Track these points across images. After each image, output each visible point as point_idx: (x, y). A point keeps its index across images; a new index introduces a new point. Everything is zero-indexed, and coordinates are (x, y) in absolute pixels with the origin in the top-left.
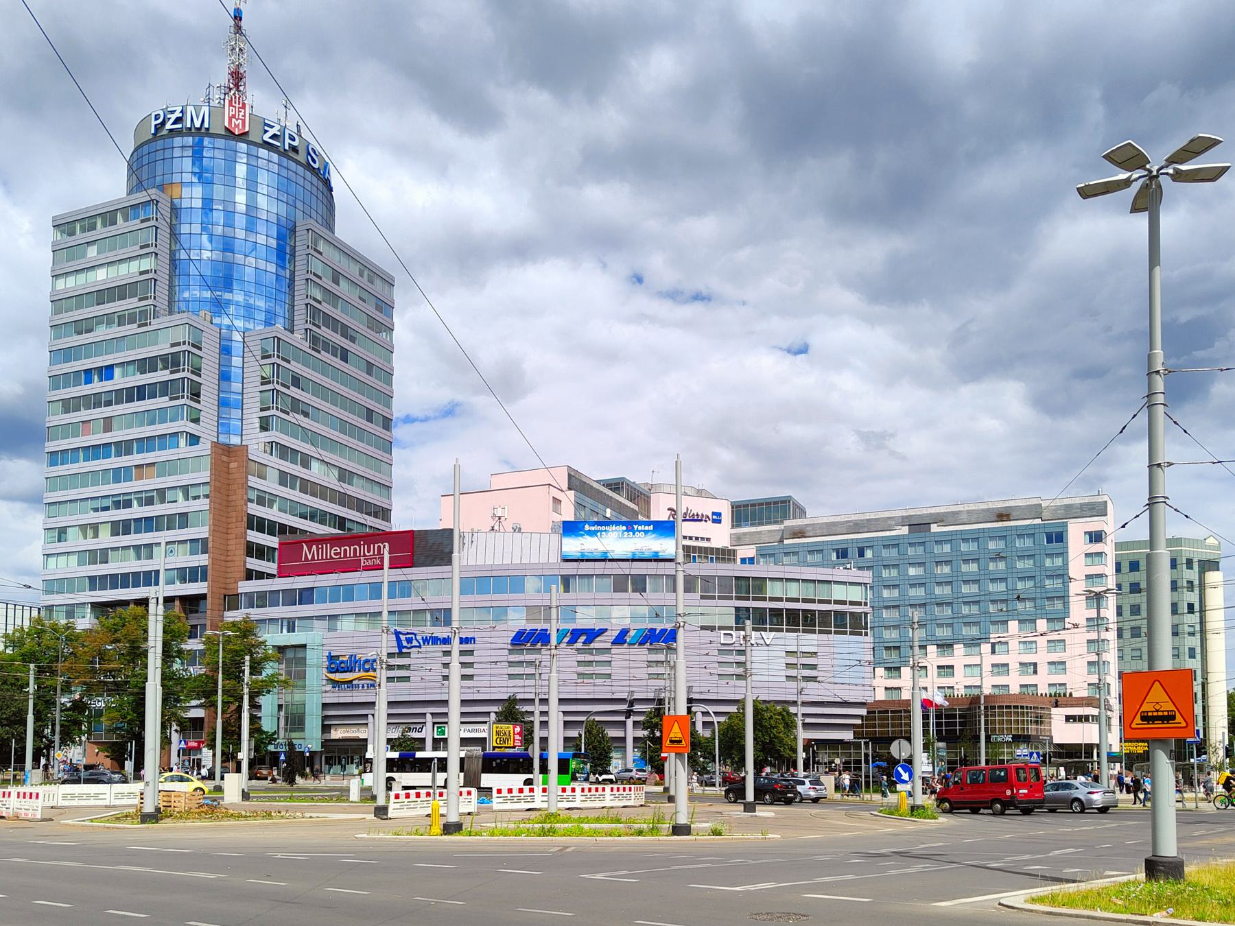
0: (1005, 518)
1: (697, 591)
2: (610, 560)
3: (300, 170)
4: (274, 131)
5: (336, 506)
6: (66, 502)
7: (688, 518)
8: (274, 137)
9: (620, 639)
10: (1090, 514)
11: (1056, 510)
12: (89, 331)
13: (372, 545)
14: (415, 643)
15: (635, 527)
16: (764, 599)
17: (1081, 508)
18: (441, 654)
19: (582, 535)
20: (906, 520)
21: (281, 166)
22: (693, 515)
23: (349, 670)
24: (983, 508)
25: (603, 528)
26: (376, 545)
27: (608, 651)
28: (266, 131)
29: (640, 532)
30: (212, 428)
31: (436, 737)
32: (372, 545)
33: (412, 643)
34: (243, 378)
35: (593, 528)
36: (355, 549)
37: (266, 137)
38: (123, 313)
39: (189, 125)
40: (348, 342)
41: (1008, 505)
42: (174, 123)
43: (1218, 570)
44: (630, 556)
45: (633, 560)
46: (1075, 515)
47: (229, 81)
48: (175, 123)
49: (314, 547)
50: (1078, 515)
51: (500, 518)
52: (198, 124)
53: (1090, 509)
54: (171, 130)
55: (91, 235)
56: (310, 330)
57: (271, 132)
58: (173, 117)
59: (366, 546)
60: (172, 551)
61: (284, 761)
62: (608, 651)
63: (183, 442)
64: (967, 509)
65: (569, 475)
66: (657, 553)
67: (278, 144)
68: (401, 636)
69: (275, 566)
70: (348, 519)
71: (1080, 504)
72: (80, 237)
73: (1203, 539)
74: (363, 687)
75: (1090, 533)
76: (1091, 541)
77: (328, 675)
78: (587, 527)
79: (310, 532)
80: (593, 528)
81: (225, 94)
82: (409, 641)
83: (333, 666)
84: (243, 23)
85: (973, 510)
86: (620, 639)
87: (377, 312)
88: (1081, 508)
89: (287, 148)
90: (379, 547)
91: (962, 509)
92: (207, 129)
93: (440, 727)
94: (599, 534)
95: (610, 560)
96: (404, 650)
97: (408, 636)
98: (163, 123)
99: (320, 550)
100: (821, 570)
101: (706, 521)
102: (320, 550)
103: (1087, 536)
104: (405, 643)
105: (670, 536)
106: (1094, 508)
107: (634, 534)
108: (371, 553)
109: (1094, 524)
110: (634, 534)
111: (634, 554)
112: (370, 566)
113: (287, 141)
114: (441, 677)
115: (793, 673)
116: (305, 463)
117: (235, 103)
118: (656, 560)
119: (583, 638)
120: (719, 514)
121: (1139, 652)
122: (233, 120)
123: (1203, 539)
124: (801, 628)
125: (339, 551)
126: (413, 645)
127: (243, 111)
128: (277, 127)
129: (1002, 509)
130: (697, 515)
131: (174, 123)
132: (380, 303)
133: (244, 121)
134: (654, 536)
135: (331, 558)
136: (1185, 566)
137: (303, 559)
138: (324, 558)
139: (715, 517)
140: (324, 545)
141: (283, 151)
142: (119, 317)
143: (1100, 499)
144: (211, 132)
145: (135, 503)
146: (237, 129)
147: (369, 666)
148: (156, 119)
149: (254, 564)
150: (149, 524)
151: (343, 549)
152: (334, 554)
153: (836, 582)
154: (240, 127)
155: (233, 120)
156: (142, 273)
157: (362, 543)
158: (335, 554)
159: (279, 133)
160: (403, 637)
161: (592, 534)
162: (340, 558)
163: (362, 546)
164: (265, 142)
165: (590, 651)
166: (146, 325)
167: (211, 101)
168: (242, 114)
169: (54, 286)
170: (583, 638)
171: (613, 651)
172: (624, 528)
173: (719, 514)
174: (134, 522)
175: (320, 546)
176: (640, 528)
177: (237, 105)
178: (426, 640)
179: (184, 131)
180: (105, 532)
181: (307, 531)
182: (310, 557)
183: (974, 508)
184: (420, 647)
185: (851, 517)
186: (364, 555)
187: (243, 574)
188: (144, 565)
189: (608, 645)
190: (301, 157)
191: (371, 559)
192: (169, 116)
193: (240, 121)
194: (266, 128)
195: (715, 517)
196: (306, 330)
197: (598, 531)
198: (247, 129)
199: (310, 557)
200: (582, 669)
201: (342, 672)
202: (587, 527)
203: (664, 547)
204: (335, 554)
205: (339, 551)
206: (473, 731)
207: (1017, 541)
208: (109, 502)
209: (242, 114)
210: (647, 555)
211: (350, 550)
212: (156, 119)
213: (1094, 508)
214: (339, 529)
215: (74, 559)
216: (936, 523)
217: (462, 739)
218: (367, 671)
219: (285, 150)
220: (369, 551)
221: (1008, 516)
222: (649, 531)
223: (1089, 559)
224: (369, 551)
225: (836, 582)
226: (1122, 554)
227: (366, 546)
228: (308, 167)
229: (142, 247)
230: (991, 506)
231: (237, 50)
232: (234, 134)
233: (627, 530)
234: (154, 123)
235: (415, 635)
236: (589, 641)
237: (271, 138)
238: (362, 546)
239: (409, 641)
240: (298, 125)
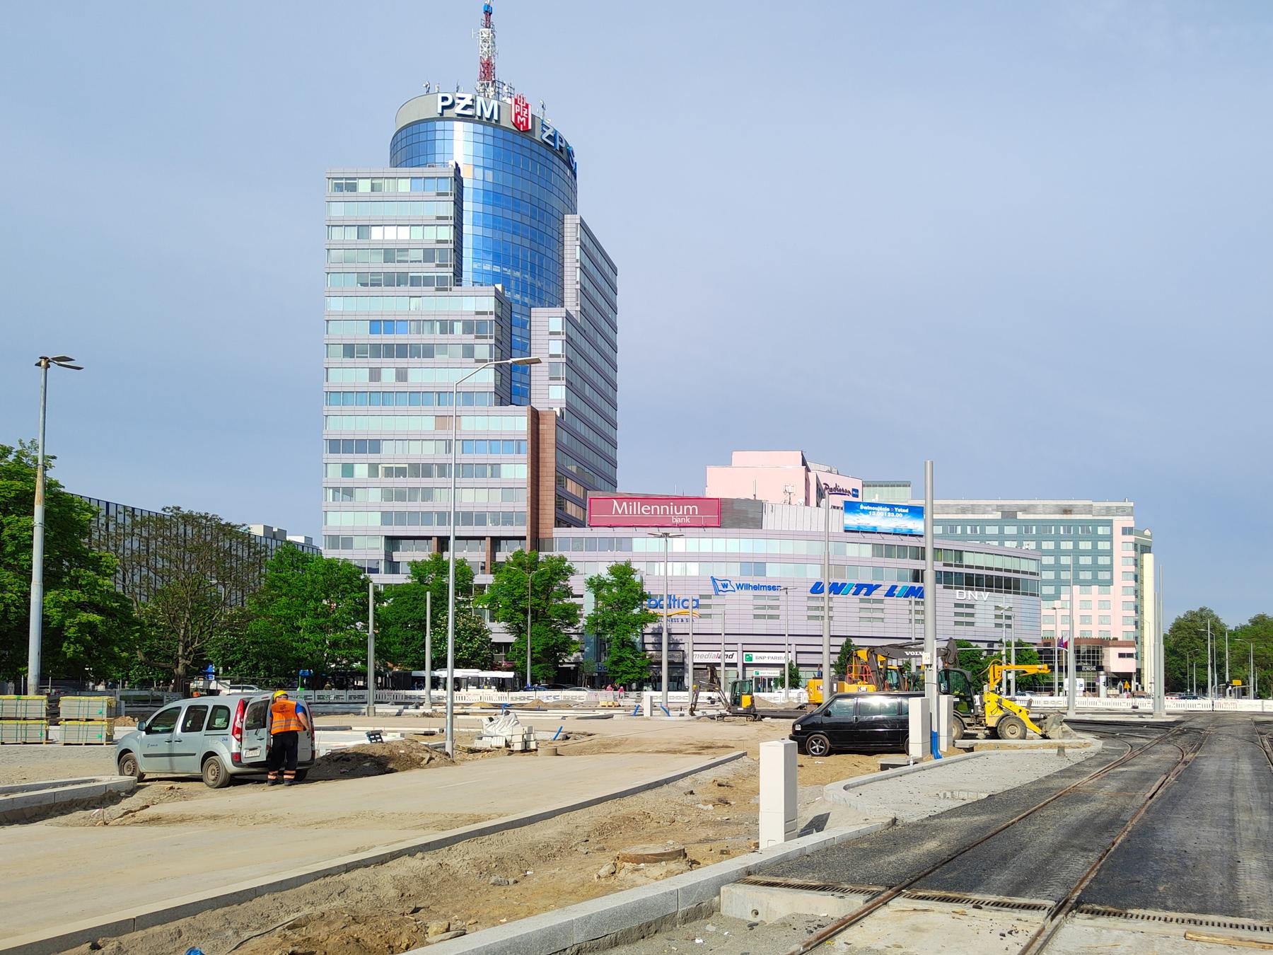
1: (940, 559)
8: (549, 137)
9: (890, 593)
11: (1101, 509)
13: (681, 507)
14: (730, 588)
15: (896, 509)
16: (962, 566)
19: (858, 513)
25: (874, 508)
26: (685, 507)
27: (881, 601)
29: (899, 513)
31: (745, 662)
32: (681, 507)
33: (727, 587)
35: (866, 508)
36: (665, 509)
41: (1071, 503)
43: (1150, 553)
45: (894, 534)
48: (464, 108)
49: (625, 504)
51: (790, 493)
52: (487, 115)
59: (675, 507)
62: (881, 601)
66: (875, 527)
68: (716, 581)
74: (682, 621)
78: (862, 507)
80: (866, 508)
86: (890, 593)
90: (688, 509)
93: (748, 655)
94: (870, 512)
96: (720, 593)
97: (723, 582)
98: (452, 106)
99: (631, 507)
100: (945, 541)
102: (631, 507)
105: (919, 518)
108: (681, 513)
111: (895, 529)
113: (558, 143)
114: (753, 616)
115: (999, 621)
117: (520, 101)
118: (910, 535)
119: (864, 591)
120: (857, 491)
124: (1012, 590)
125: (649, 509)
127: (526, 110)
133: (527, 119)
134: (909, 517)
137: (613, 513)
138: (635, 513)
139: (854, 493)
140: (635, 503)
146: (521, 126)
151: (653, 507)
152: (645, 511)
153: (1022, 558)
154: (525, 124)
155: (519, 117)
156: (439, 242)
157: (672, 504)
162: (651, 514)
163: (672, 507)
164: (459, 115)
165: (868, 601)
168: (525, 112)
170: (864, 591)
171: (885, 602)
172: (888, 509)
173: (857, 491)
175: (631, 504)
176: (899, 510)
178: (740, 587)
182: (620, 512)
184: (734, 591)
186: (674, 514)
189: (882, 597)
190: (564, 156)
191: (681, 518)
193: (524, 119)
195: (854, 493)
197: (870, 510)
199: (620, 512)
200: (863, 614)
202: (862, 507)
205: (649, 509)
206: (776, 658)
209: (525, 112)
210: (904, 531)
211: (660, 510)
217: (737, 667)
220: (678, 511)
221: (1070, 511)
222: (905, 513)
224: (678, 511)
225: (1022, 558)
227: (675, 507)
233: (891, 512)
236: (867, 594)
238: (672, 507)
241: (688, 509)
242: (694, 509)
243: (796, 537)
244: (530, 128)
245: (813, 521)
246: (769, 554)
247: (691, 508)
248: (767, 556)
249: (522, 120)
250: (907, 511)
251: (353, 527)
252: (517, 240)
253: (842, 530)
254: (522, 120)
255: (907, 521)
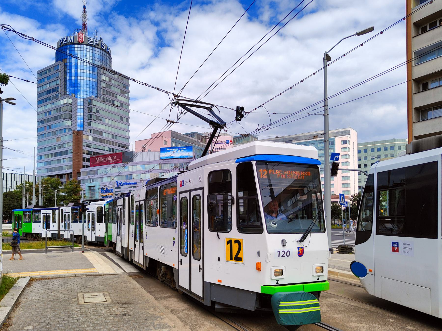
0: (316, 137)
2: (174, 159)
3: (99, 50)
4: (91, 40)
5: (111, 146)
6: (46, 147)
7: (218, 143)
8: (91, 42)
10: (345, 134)
11: (334, 134)
12: (46, 102)
14: (122, 185)
15: (181, 149)
17: (342, 133)
18: (128, 187)
19: (166, 152)
20: (284, 140)
21: (94, 50)
22: (220, 142)
23: (106, 192)
24: (309, 134)
25: (172, 149)
26: (113, 157)
28: (89, 41)
29: (182, 150)
30: (75, 126)
34: (84, 111)
35: (169, 150)
37: (89, 43)
38: (53, 96)
39: (68, 42)
40: (114, 98)
41: (317, 133)
42: (65, 42)
44: (179, 157)
45: (180, 159)
46: (339, 135)
47: (82, 27)
50: (341, 135)
52: (70, 41)
53: (344, 133)
54: (64, 44)
55: (46, 75)
56: (102, 96)
57: (90, 41)
58: (64, 40)
60: (65, 161)
61: (335, 204)
63: (67, 130)
64: (304, 135)
65: (171, 133)
67: (92, 44)
69: (89, 163)
70: (115, 149)
71: (341, 131)
72: (44, 76)
73: (405, 139)
75: (343, 141)
76: (343, 144)
77: (101, 194)
78: (167, 149)
79: (103, 154)
80: (169, 150)
81: (79, 31)
82: (120, 184)
83: (102, 191)
84: (86, 10)
85: (306, 135)
87: (124, 88)
88: (342, 133)
89: (95, 44)
90: (114, 157)
91: (302, 135)
92: (73, 42)
95: (174, 159)
97: (120, 183)
101: (224, 143)
103: (342, 142)
104: (119, 185)
105: (190, 151)
106: (346, 133)
107: (181, 151)
109: (344, 138)
110: (181, 151)
112: (111, 163)
113: (95, 42)
116: (101, 133)
121: (361, 180)
122: (80, 39)
123: (405, 139)
126: (121, 185)
128: (92, 39)
129: (315, 135)
130: (221, 141)
131: (65, 42)
132: (125, 86)
133: (83, 39)
134: (186, 151)
135: (102, 161)
136: (397, 149)
139: (227, 142)
141: (94, 46)
142: (52, 97)
143: (348, 129)
144: (74, 43)
145: (57, 148)
147: (111, 191)
148: (61, 41)
149: (85, 163)
150: (59, 154)
155: (80, 39)
156: (57, 85)
158: (103, 160)
159: (92, 41)
160: (118, 183)
161: (168, 151)
162: (104, 161)
166: (58, 99)
167: (75, 34)
168: (82, 37)
169: (38, 90)
172: (178, 149)
174: (57, 153)
177: (81, 35)
178: (124, 184)
179: (67, 44)
180: (50, 156)
181: (102, 153)
182: (97, 161)
183: (306, 135)
184: (123, 186)
185: (303, 134)
187: (82, 167)
188: (59, 165)
190: (99, 47)
191: (112, 161)
192: (63, 40)
193: (82, 39)
194: (89, 40)
195: (227, 142)
196: (101, 96)
198: (83, 41)
199: (97, 161)
201: (105, 193)
202: (167, 149)
203: (189, 154)
204: (103, 160)
207: (319, 145)
208: (50, 148)
209: (82, 37)
212: (61, 41)
213: (346, 133)
214: (112, 152)
215: (43, 164)
216: (294, 140)
218: (110, 193)
219: (95, 45)
220: (111, 159)
222: (185, 149)
223: (343, 150)
224: (111, 159)
226: (390, 144)
228: (102, 49)
229: (57, 78)
230: (312, 134)
231: (84, 17)
232: (80, 43)
233: (179, 150)
234: (60, 42)
235: (122, 182)
237: (90, 42)
239: (120, 184)
240: (100, 37)
241: (114, 157)
242: (115, 157)
243: (142, 164)
244: (83, 41)
245: (150, 157)
246: (133, 171)
247: (114, 157)
248: (132, 172)
249: (81, 39)
250: (186, 149)
251: (141, 170)
252: (91, 79)
253: (158, 159)
254: (81, 39)
255: (186, 153)
